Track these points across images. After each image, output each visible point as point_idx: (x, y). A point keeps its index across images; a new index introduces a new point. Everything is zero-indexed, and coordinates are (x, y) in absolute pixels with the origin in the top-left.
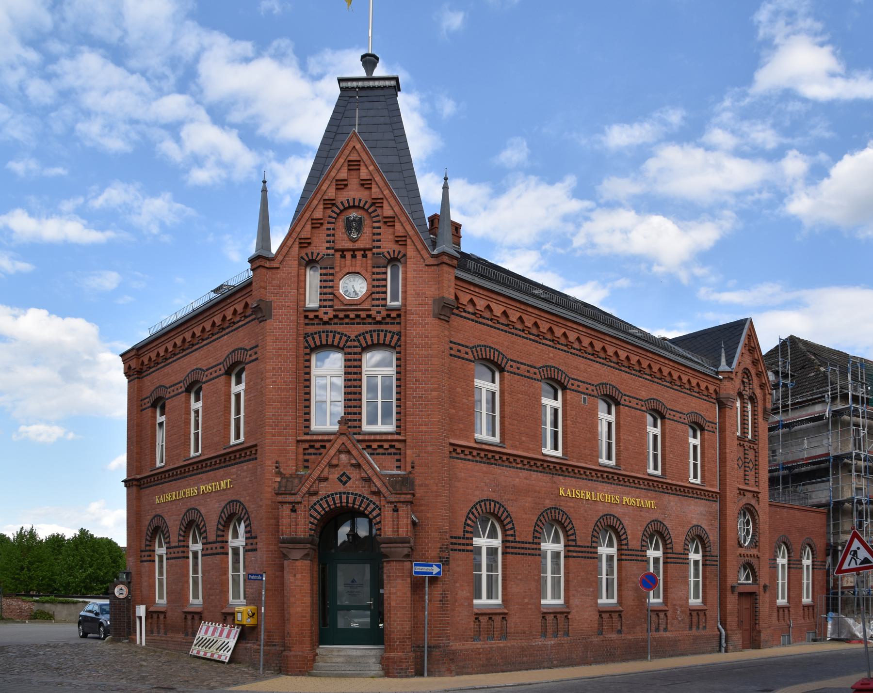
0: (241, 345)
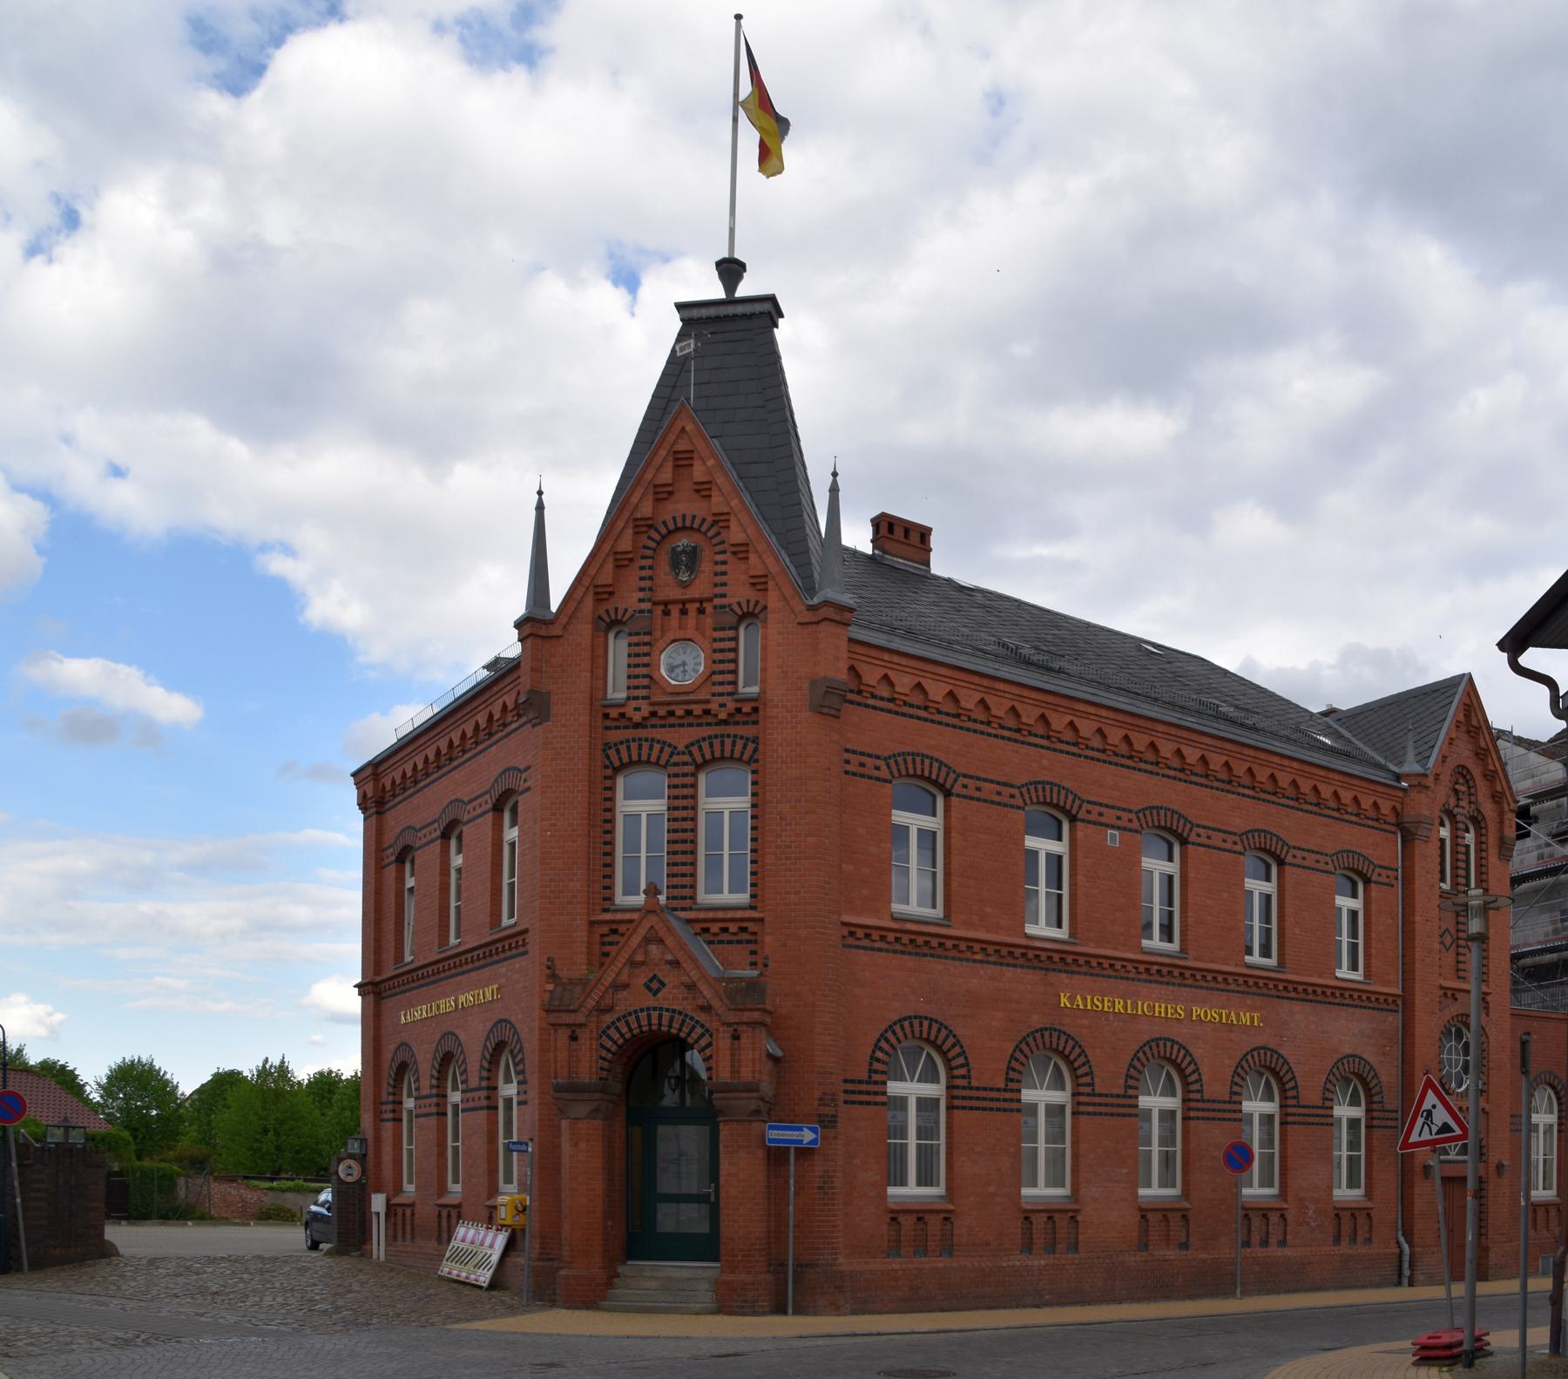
0: (514, 763)
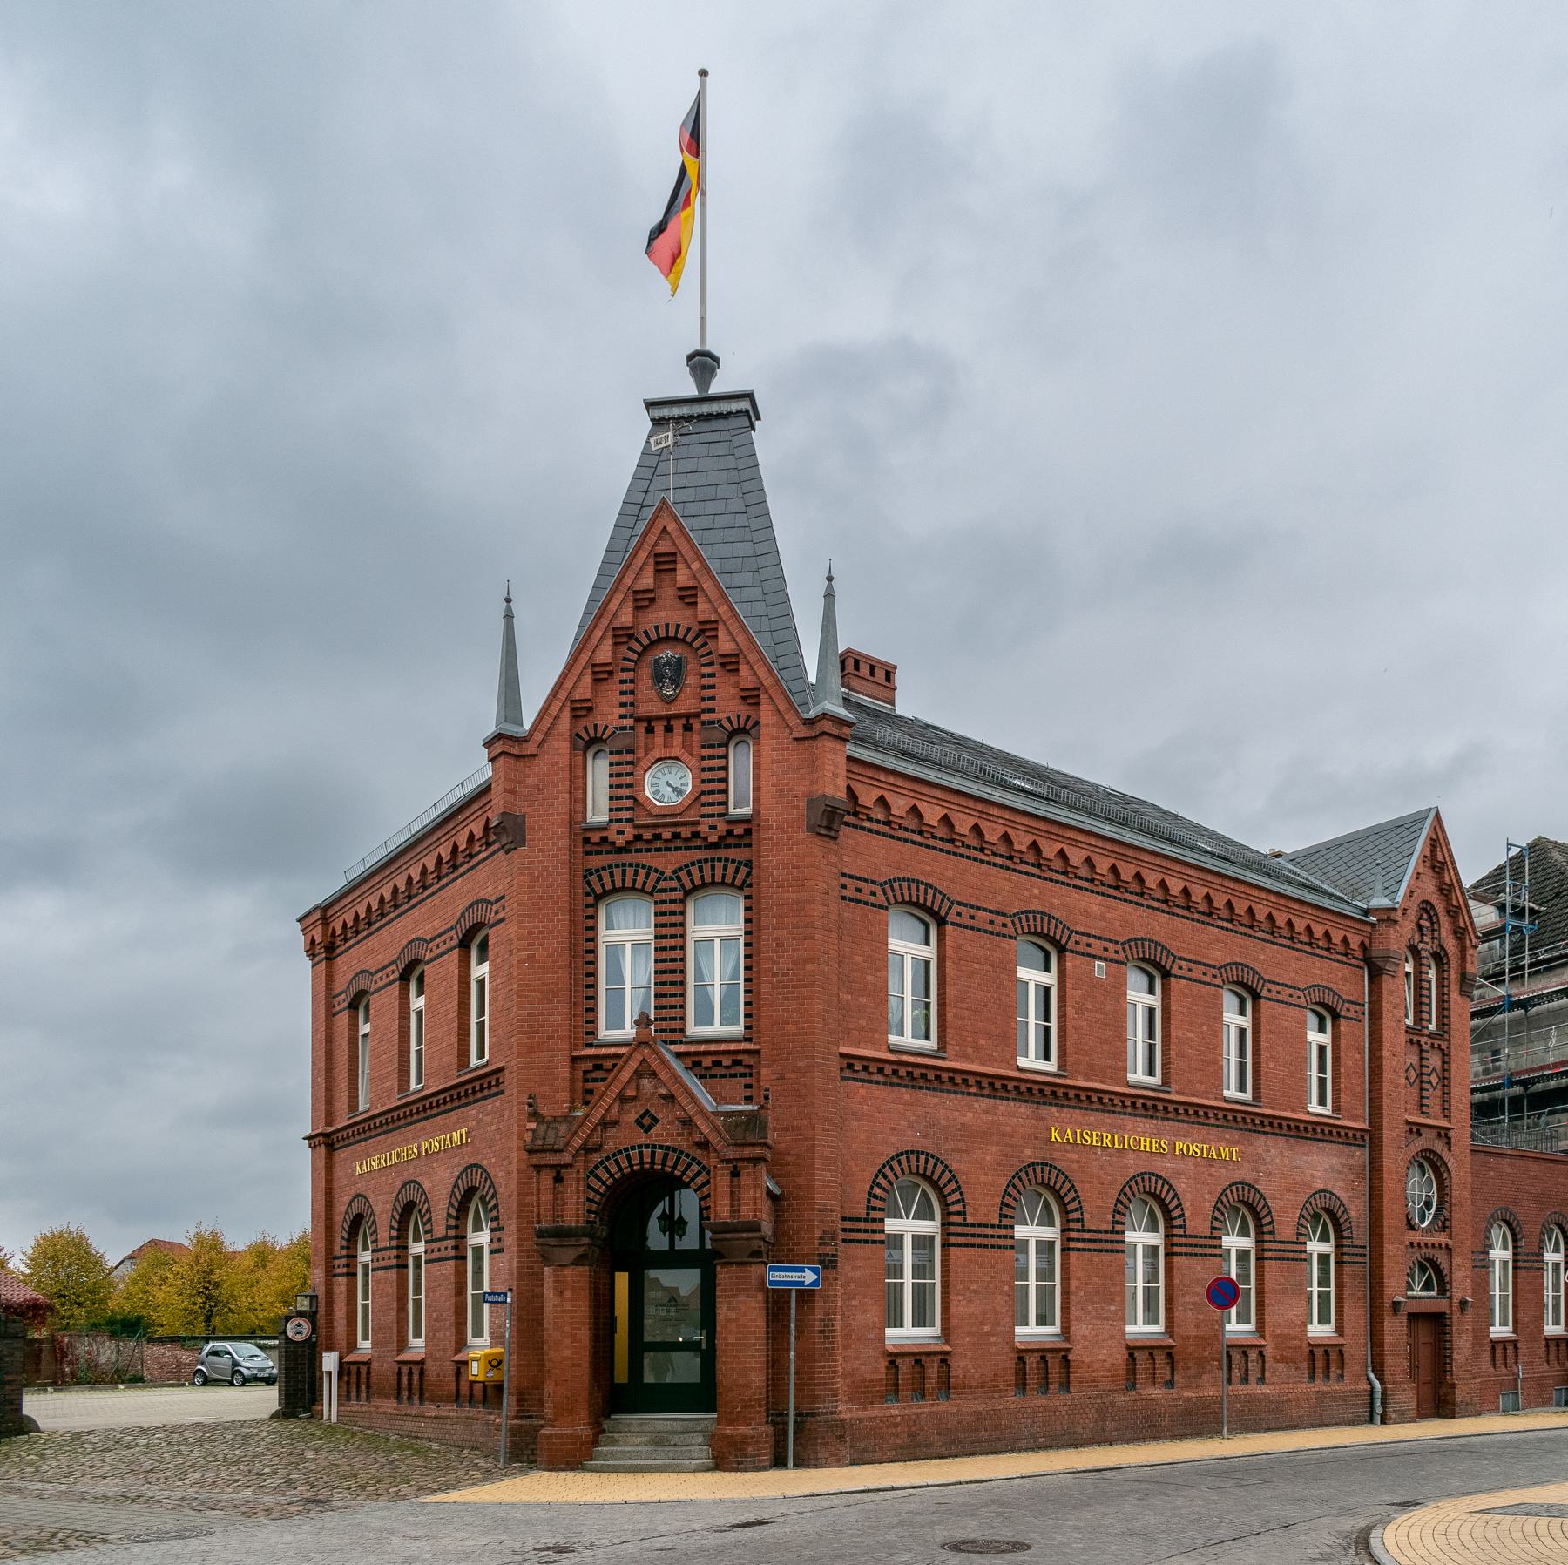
0: (482, 895)
